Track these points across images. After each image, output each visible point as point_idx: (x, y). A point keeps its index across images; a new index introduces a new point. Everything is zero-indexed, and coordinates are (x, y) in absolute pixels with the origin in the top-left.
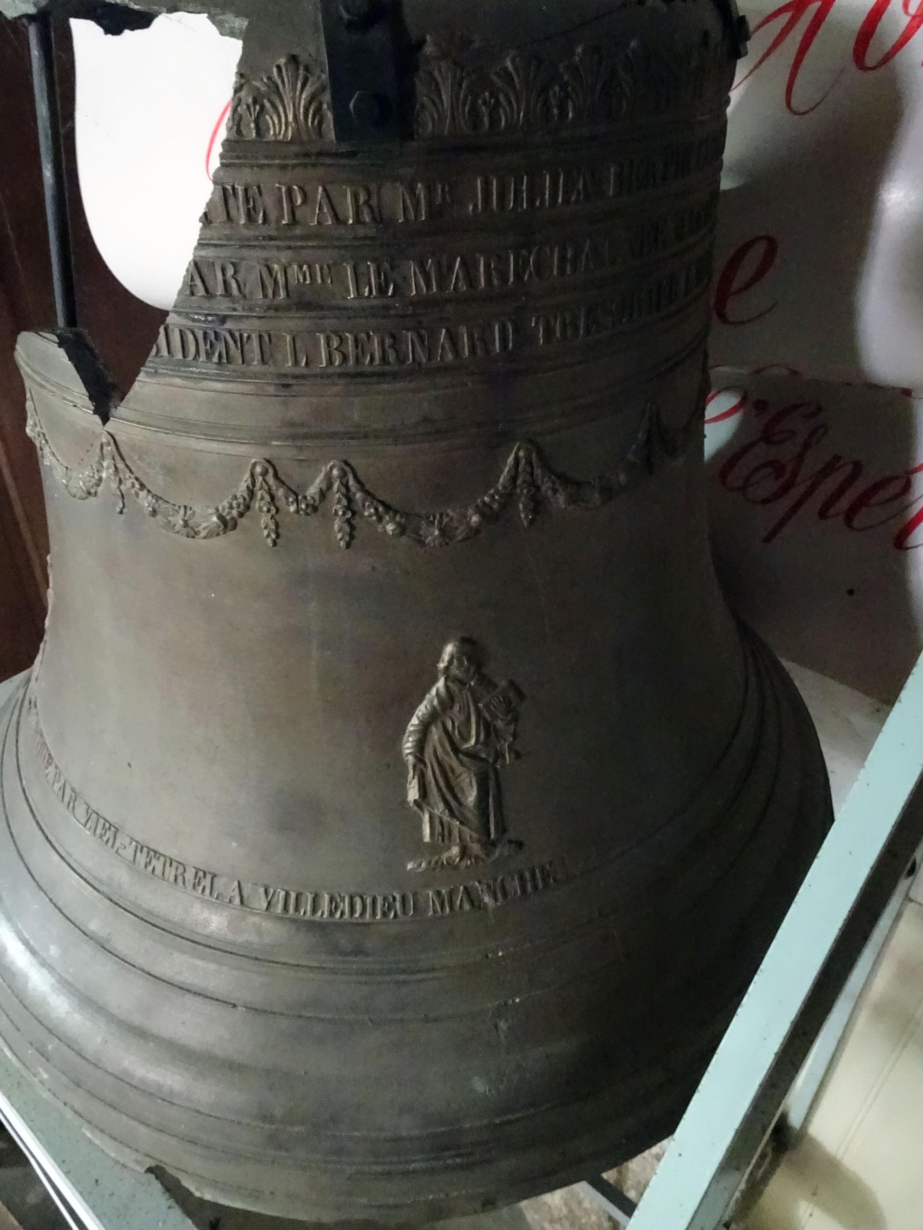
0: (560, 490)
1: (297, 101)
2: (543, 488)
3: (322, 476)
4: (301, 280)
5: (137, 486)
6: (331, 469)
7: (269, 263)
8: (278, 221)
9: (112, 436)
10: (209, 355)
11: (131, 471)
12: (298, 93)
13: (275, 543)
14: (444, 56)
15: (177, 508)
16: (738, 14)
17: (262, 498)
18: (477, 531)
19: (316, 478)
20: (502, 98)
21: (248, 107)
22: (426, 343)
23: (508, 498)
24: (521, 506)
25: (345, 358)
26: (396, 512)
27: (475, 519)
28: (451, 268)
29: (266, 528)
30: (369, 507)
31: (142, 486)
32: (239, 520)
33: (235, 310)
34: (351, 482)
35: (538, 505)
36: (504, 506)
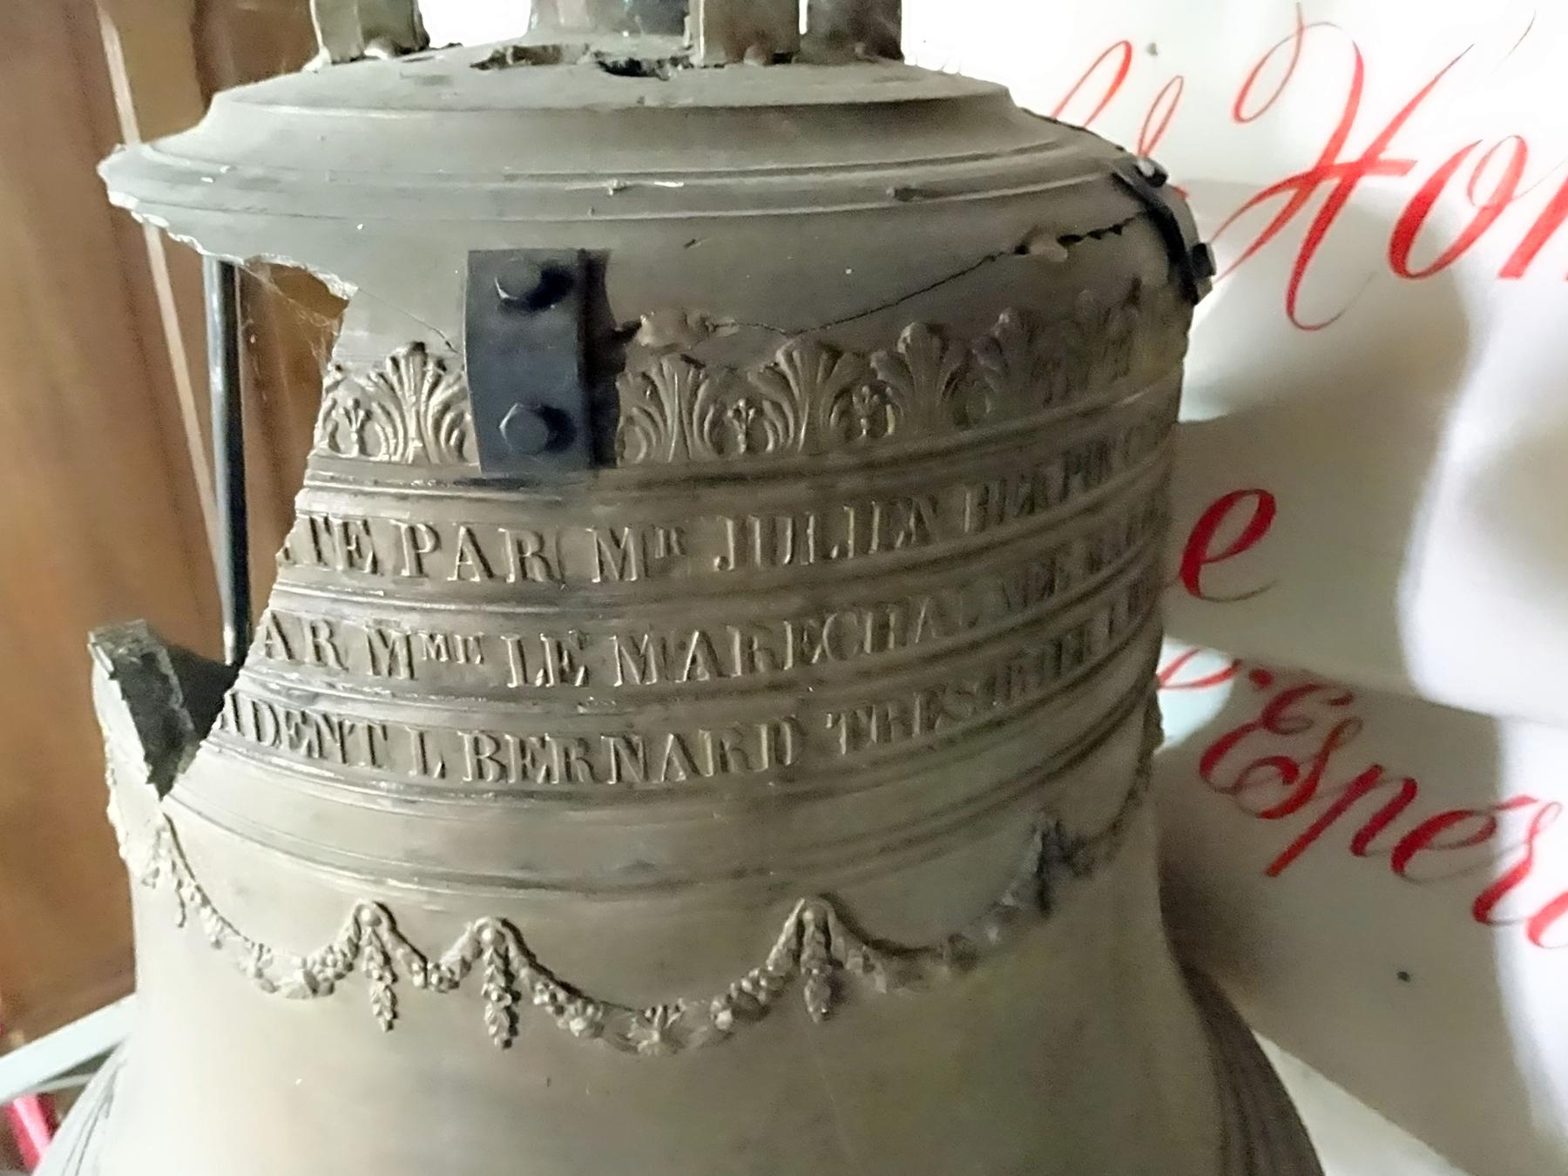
0: (879, 966)
1: (423, 409)
2: (848, 966)
3: (463, 939)
4: (433, 655)
5: (198, 898)
6: (480, 929)
7: (383, 628)
8: (397, 570)
9: (170, 821)
10: (294, 745)
11: (192, 876)
12: (424, 398)
13: (390, 1026)
14: (669, 349)
15: (249, 945)
16: (1196, 237)
17: (371, 958)
18: (728, 1035)
19: (455, 939)
20: (767, 406)
21: (347, 413)
22: (641, 754)
23: (785, 983)
24: (807, 993)
25: (504, 770)
26: (588, 1001)
27: (724, 1017)
28: (683, 647)
29: (377, 1001)
30: (541, 992)
31: (206, 901)
32: (338, 983)
33: (332, 686)
34: (513, 952)
35: (837, 990)
36: (775, 994)
